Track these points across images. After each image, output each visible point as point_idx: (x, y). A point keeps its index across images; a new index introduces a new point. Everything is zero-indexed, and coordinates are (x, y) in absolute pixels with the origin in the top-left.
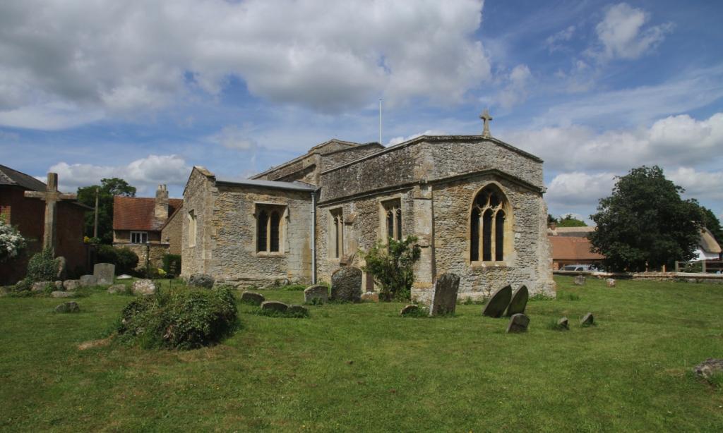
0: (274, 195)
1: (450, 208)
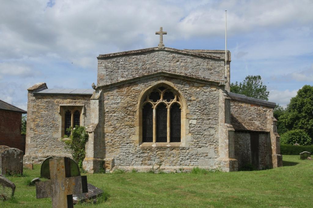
0: (75, 99)
1: (120, 104)
